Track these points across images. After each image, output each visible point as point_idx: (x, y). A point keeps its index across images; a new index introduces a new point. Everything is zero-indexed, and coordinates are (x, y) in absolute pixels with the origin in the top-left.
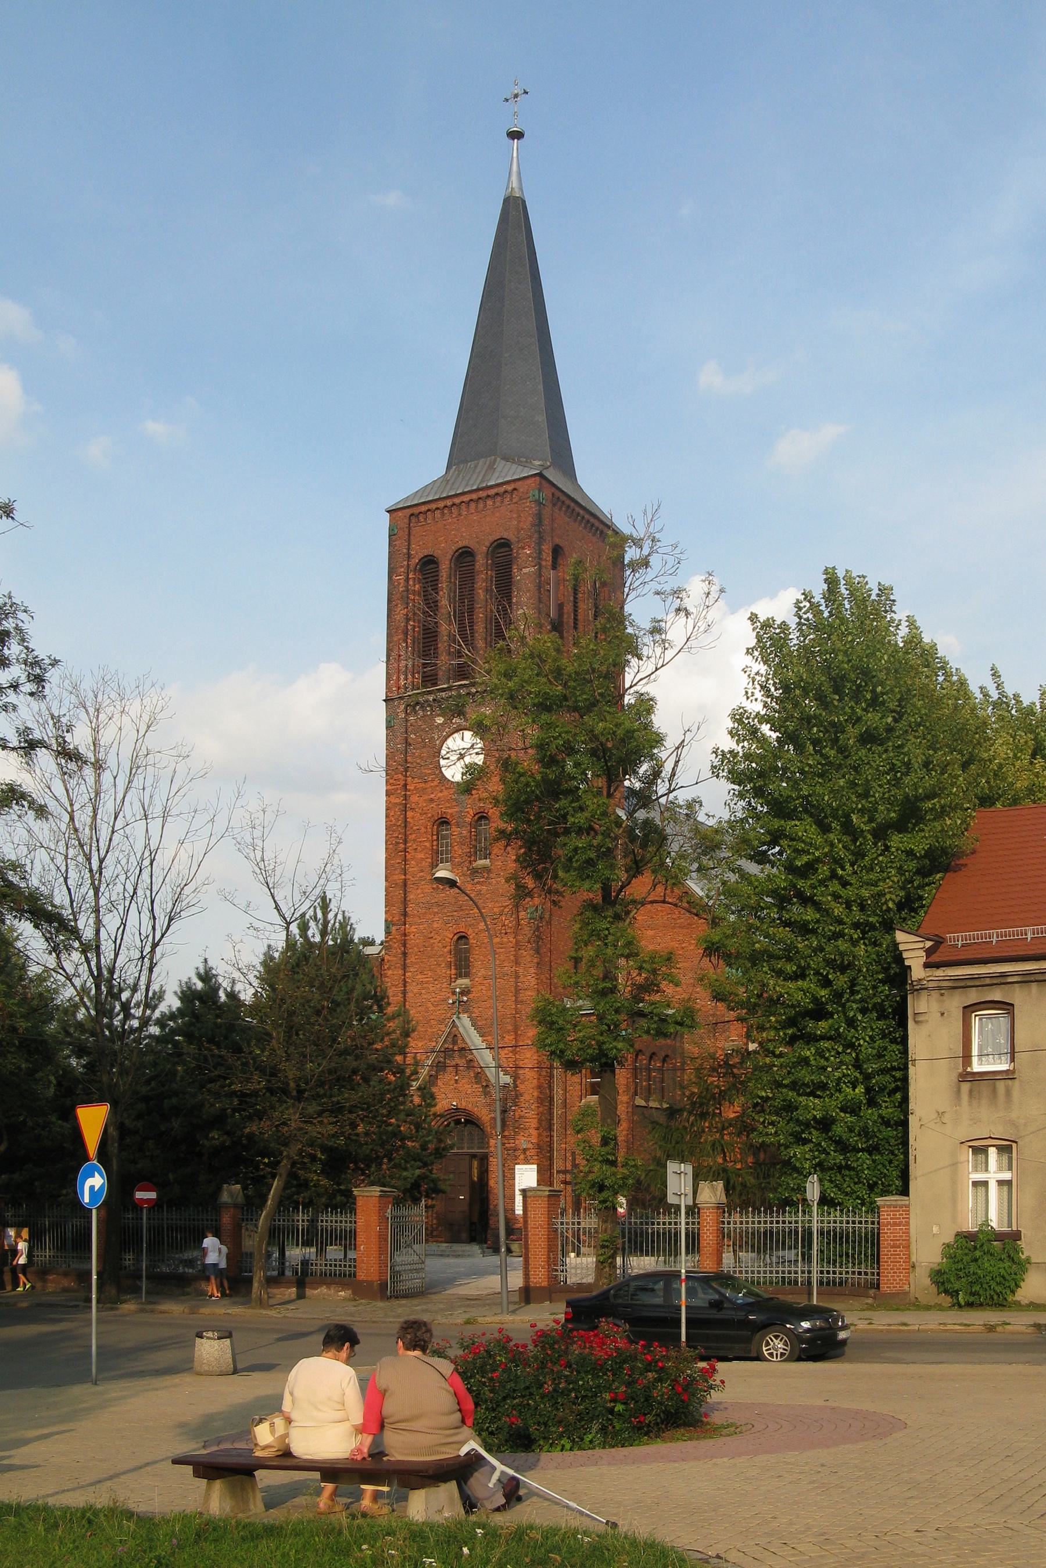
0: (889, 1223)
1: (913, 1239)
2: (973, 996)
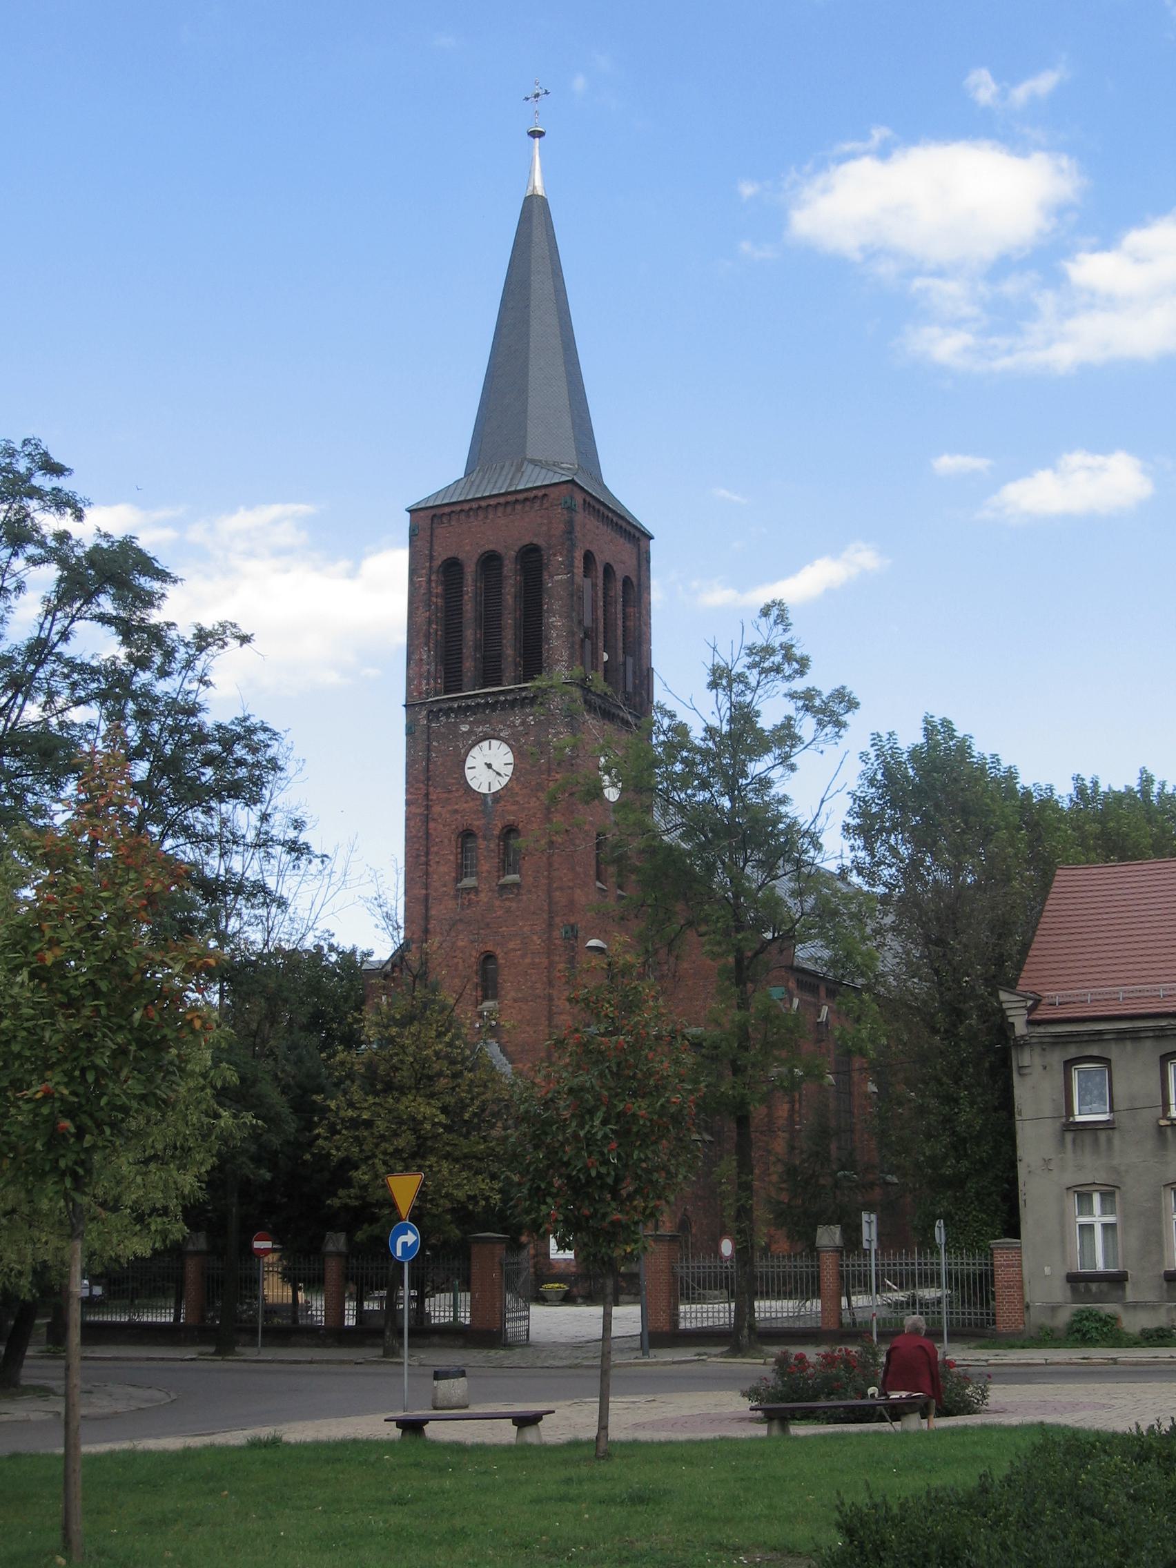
0: (1002, 1265)
1: (1026, 1281)
2: (1073, 1052)
